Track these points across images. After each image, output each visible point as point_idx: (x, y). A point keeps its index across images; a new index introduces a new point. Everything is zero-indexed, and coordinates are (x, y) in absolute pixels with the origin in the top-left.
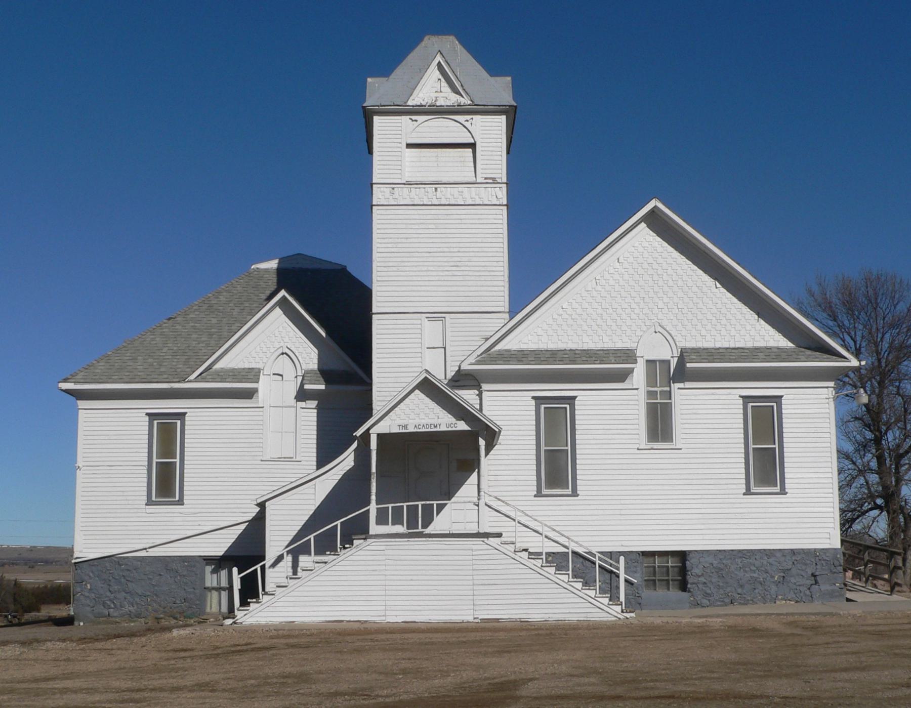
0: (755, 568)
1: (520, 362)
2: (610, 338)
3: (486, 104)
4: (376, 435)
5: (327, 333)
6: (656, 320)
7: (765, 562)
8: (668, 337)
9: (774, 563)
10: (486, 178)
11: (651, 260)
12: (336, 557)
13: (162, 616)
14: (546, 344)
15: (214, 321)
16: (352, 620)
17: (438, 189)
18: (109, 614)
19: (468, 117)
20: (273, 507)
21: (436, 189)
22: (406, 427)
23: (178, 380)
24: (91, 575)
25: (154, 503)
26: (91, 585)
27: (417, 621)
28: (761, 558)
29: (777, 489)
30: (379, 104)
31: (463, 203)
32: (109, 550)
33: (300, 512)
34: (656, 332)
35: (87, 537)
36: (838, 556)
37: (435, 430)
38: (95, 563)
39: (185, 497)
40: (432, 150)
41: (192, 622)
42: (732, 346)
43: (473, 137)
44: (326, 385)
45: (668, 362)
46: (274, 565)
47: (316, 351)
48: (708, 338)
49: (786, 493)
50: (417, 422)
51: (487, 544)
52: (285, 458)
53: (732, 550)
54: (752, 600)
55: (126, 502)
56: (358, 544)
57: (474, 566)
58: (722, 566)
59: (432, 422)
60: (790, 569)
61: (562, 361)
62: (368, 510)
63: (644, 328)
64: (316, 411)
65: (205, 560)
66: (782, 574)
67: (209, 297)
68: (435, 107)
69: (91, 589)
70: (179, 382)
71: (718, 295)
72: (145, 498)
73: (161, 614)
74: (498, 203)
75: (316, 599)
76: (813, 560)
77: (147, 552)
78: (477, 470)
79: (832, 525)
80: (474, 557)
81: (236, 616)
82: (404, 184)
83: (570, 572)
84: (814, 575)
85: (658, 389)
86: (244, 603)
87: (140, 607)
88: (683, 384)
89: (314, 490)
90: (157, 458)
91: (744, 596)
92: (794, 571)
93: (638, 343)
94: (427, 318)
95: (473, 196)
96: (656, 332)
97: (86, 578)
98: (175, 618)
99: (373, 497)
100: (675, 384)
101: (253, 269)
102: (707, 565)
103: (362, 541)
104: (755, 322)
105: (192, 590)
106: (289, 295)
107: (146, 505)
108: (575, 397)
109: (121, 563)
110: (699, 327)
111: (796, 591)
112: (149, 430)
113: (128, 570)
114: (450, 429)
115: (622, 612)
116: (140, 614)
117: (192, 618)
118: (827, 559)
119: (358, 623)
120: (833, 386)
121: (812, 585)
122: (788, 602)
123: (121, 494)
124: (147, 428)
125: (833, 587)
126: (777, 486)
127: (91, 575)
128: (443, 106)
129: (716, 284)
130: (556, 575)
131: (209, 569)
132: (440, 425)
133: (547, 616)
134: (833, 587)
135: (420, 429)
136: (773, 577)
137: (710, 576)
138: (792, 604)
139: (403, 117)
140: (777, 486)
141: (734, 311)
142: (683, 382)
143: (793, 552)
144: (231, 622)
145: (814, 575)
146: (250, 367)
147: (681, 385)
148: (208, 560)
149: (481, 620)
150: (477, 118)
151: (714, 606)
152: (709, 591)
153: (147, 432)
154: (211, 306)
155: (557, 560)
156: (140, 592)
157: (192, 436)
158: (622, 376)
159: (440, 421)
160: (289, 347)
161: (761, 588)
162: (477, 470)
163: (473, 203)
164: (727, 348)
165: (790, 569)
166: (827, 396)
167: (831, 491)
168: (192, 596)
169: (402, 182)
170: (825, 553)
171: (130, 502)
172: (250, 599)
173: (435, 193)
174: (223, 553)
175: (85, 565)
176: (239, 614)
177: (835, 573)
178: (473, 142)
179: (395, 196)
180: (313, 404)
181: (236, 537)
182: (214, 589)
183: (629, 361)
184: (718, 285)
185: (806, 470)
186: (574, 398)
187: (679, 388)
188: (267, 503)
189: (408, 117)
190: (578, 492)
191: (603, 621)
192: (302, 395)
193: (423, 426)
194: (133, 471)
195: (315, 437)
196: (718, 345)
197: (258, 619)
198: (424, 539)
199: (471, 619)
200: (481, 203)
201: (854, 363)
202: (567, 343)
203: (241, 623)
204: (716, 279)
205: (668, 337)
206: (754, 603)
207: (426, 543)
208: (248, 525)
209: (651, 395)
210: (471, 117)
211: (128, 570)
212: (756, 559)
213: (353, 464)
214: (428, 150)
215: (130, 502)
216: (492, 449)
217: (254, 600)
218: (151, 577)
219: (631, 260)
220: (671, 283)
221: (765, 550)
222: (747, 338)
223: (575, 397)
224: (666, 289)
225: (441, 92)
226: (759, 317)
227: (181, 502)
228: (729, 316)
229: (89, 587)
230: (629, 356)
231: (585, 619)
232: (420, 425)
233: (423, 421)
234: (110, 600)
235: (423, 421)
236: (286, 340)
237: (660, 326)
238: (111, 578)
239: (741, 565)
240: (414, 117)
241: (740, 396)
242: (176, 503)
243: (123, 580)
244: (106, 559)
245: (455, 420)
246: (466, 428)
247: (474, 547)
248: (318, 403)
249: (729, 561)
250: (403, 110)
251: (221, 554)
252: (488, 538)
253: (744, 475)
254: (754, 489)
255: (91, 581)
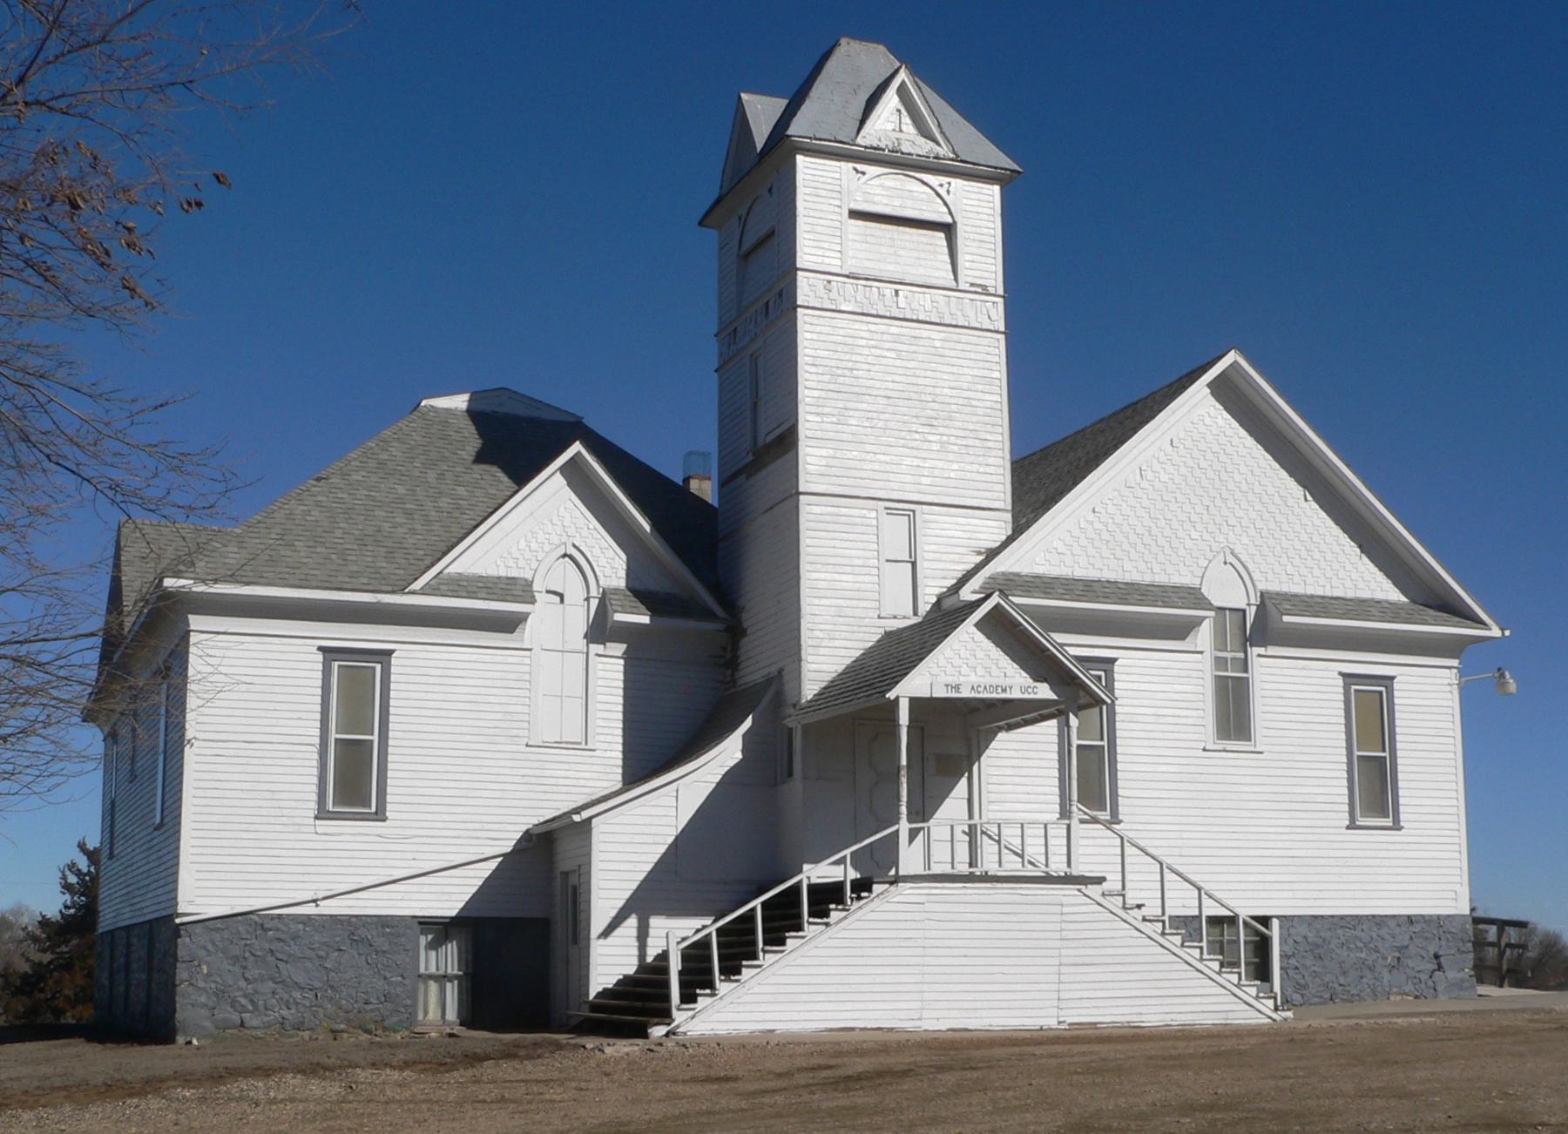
0: (1362, 945)
1: (1047, 594)
2: (1163, 567)
3: (976, 161)
4: (907, 699)
5: (654, 525)
6: (1225, 544)
7: (1375, 936)
8: (1244, 573)
9: (1387, 937)
10: (972, 285)
11: (1216, 448)
12: (844, 913)
13: (342, 1026)
14: (1070, 570)
15: (401, 490)
16: (869, 1026)
17: (901, 293)
18: (242, 1022)
19: (944, 180)
20: (603, 828)
21: (897, 292)
22: (957, 688)
23: (390, 588)
24: (210, 947)
25: (331, 816)
26: (208, 967)
27: (970, 1028)
28: (1370, 929)
29: (1388, 822)
30: (812, 136)
31: (938, 321)
32: (244, 901)
33: (650, 839)
34: (1225, 563)
35: (202, 876)
36: (1468, 927)
37: (1003, 696)
38: (219, 925)
39: (389, 807)
40: (884, 226)
41: (399, 1038)
42: (1328, 594)
43: (951, 213)
44: (651, 617)
45: (1244, 611)
46: (606, 933)
47: (624, 557)
48: (1297, 579)
49: (1400, 829)
50: (973, 679)
51: (1085, 895)
52: (567, 743)
53: (1332, 916)
54: (1358, 995)
55: (278, 812)
56: (880, 891)
57: (1064, 933)
58: (1319, 941)
59: (994, 682)
60: (1407, 947)
61: (1106, 598)
62: (897, 831)
63: (1210, 555)
64: (622, 662)
65: (420, 923)
66: (1397, 954)
67: (372, 448)
68: (899, 154)
69: (209, 975)
70: (393, 592)
71: (1309, 513)
72: (314, 806)
73: (342, 1022)
74: (991, 328)
75: (812, 989)
76: (1435, 932)
77: (317, 906)
78: (966, 775)
79: (1458, 879)
80: (1065, 918)
81: (673, 1020)
82: (847, 277)
83: (1204, 944)
84: (1437, 957)
85: (1229, 655)
86: (688, 998)
87: (302, 1010)
88: (1263, 649)
89: (674, 799)
90: (337, 733)
91: (1348, 988)
92: (1413, 950)
93: (1202, 577)
94: (886, 508)
95: (953, 311)
96: (1225, 563)
97: (202, 953)
98: (368, 1032)
99: (904, 809)
100: (1254, 649)
101: (425, 406)
102: (1299, 939)
103: (887, 886)
104: (1355, 559)
105: (400, 978)
106: (587, 450)
107: (316, 818)
108: (1115, 660)
109: (266, 926)
110: (1284, 560)
111: (1415, 981)
112: (323, 680)
113: (279, 940)
114: (1026, 696)
115: (1276, 1009)
116: (302, 1023)
117: (399, 1031)
118: (1453, 930)
119: (880, 1032)
120: (1456, 665)
121: (1435, 970)
122: (1405, 997)
123: (268, 795)
124: (320, 675)
125: (1461, 975)
126: (1388, 817)
127: (210, 947)
128: (911, 154)
129: (1305, 496)
130: (1185, 949)
131: (423, 941)
132: (1011, 688)
133: (1168, 1017)
134: (1461, 975)
135: (979, 692)
136: (1385, 958)
137: (1303, 957)
138: (1410, 1001)
139: (843, 163)
140: (1388, 817)
141: (1329, 539)
142: (1265, 646)
143: (1410, 919)
144: (664, 1032)
145: (1437, 957)
146: (509, 575)
147: (1261, 651)
148: (426, 924)
149: (1069, 1024)
150: (957, 183)
151: (1311, 1004)
152: (1302, 982)
153: (319, 683)
154: (382, 464)
155: (1187, 926)
156: (301, 980)
157: (403, 695)
158: (1179, 630)
159: (1008, 682)
160: (577, 544)
161: (1370, 977)
162: (966, 775)
163: (954, 323)
164: (1323, 597)
165: (1407, 947)
166: (1449, 681)
167: (1456, 826)
168: (399, 990)
169: (843, 272)
170: (1451, 922)
171: (285, 812)
172: (701, 988)
173: (895, 299)
174: (457, 911)
175: (198, 929)
176: (679, 1017)
177: (1463, 952)
178: (949, 220)
179: (834, 295)
180: (619, 649)
181: (480, 883)
182: (431, 977)
183: (460, 594)
184: (1309, 497)
185: (1425, 793)
186: (1112, 661)
187: (1259, 655)
188: (594, 821)
189: (851, 165)
190: (1121, 817)
191: (1249, 1025)
192: (600, 630)
193: (985, 688)
194: (291, 755)
195: (620, 708)
196: (1310, 591)
197: (716, 1025)
198: (989, 885)
199: (1053, 1023)
200: (967, 324)
201: (1496, 632)
202: (1101, 570)
203: (685, 1034)
204: (1304, 487)
205: (1244, 573)
206: (1361, 999)
207: (992, 892)
208: (501, 863)
209: (1220, 663)
210: (948, 179)
211: (279, 940)
212: (1363, 930)
213: (739, 756)
214: (878, 225)
215: (285, 812)
216: (993, 739)
217: (708, 991)
218: (322, 953)
219: (1189, 444)
220: (1244, 487)
221: (1374, 916)
222: (1348, 583)
223: (1115, 660)
224: (1238, 495)
225: (901, 131)
226: (1362, 552)
227: (380, 815)
228: (1323, 547)
229: (205, 971)
230: (1194, 597)
231: (1224, 1022)
232: (979, 686)
233: (982, 680)
234: (245, 996)
235: (982, 680)
236: (571, 531)
237: (1232, 553)
238: (247, 954)
239: (1343, 939)
240: (860, 167)
241: (1340, 674)
242: (371, 817)
243: (270, 958)
244: (239, 918)
245: (1031, 681)
246: (1051, 695)
247: (1065, 900)
248: (628, 648)
249: (1329, 933)
250: (839, 151)
251: (453, 913)
252: (1086, 885)
253: (1347, 797)
254: (1361, 821)
255: (208, 959)
